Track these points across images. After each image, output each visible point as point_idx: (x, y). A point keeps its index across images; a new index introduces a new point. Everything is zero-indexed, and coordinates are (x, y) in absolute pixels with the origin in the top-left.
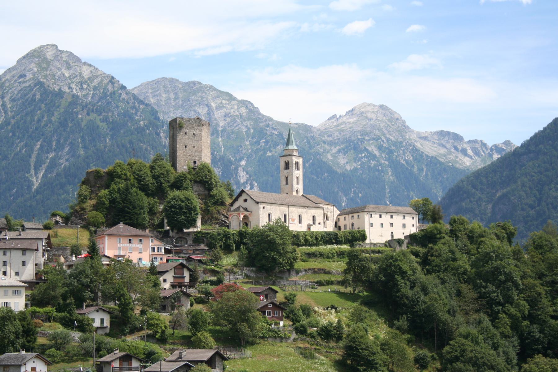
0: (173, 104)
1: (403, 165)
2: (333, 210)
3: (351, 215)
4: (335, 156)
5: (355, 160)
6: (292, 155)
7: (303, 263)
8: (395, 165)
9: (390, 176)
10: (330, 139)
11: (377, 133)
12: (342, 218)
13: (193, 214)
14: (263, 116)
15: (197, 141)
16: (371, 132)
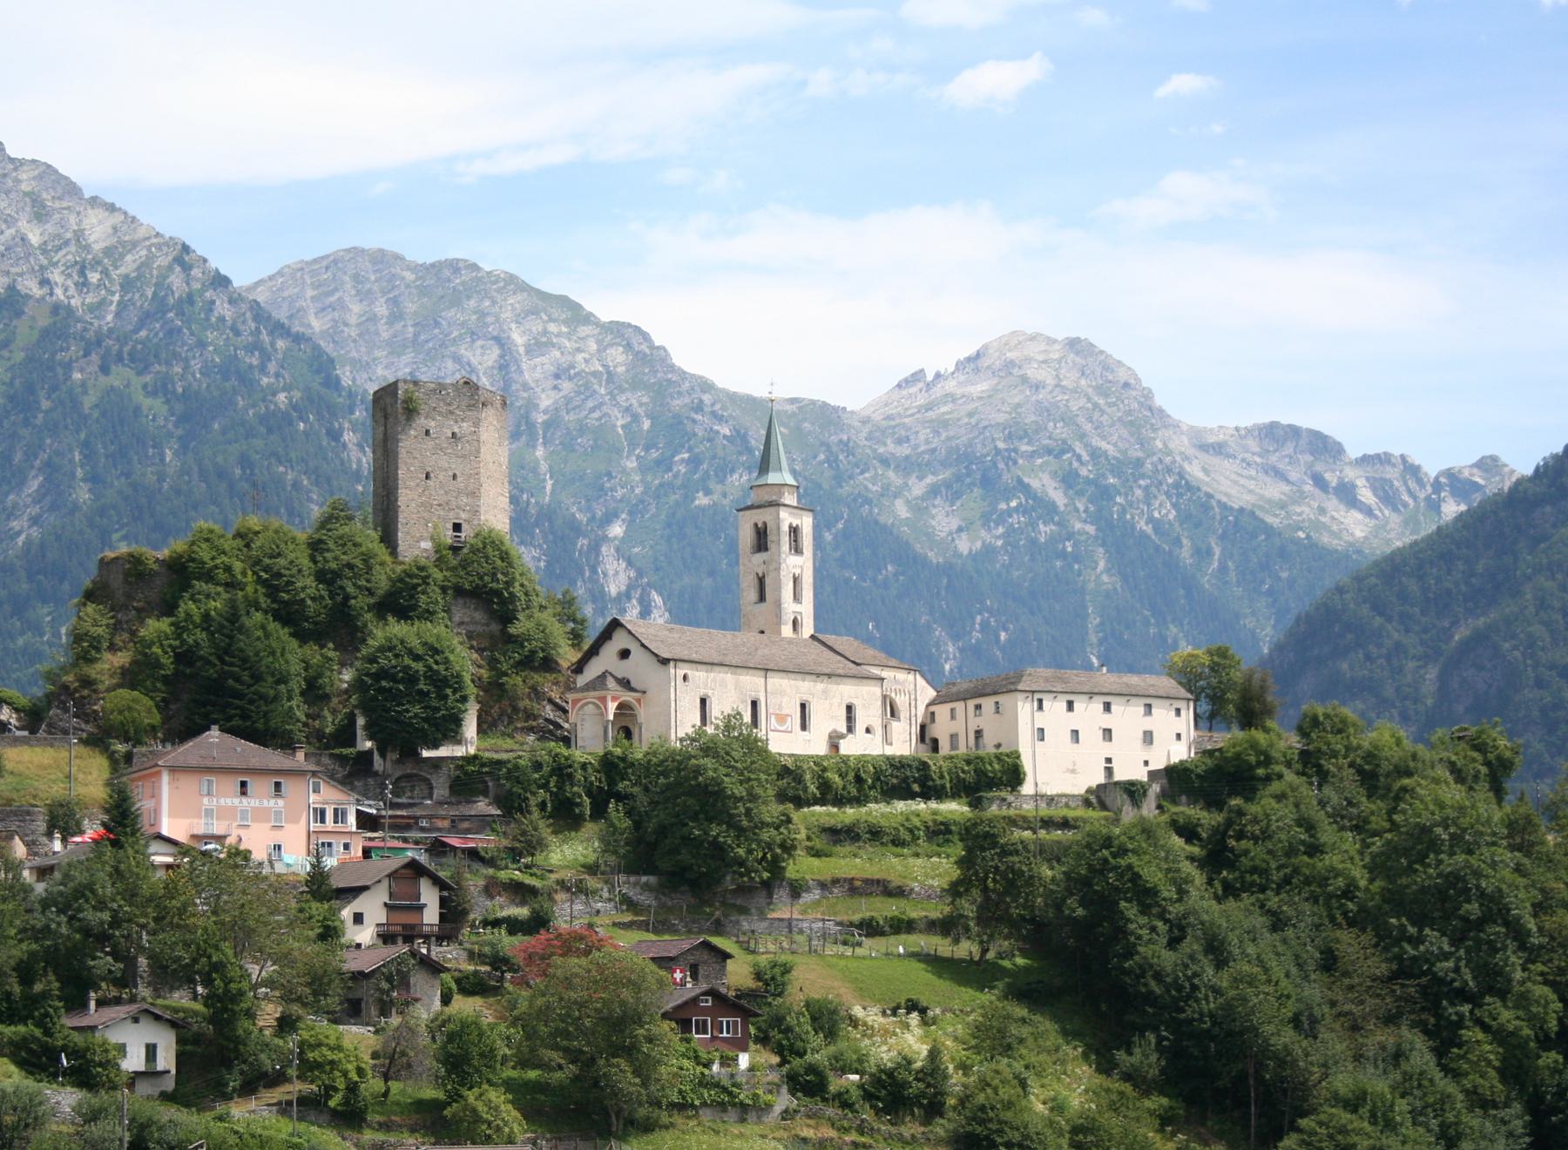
0: (385, 335)
1: (1143, 534)
2: (912, 687)
3: (971, 704)
4: (920, 508)
5: (986, 520)
6: (779, 505)
7: (815, 862)
8: (1117, 536)
9: (1101, 573)
10: (904, 450)
11: (1060, 431)
12: (942, 711)
13: (452, 697)
14: (683, 375)
15: (464, 456)
16: (1040, 428)
